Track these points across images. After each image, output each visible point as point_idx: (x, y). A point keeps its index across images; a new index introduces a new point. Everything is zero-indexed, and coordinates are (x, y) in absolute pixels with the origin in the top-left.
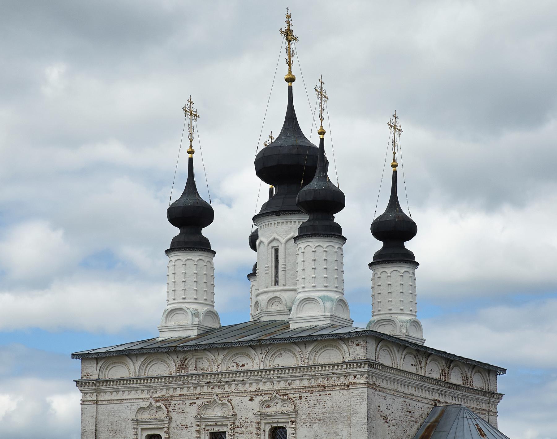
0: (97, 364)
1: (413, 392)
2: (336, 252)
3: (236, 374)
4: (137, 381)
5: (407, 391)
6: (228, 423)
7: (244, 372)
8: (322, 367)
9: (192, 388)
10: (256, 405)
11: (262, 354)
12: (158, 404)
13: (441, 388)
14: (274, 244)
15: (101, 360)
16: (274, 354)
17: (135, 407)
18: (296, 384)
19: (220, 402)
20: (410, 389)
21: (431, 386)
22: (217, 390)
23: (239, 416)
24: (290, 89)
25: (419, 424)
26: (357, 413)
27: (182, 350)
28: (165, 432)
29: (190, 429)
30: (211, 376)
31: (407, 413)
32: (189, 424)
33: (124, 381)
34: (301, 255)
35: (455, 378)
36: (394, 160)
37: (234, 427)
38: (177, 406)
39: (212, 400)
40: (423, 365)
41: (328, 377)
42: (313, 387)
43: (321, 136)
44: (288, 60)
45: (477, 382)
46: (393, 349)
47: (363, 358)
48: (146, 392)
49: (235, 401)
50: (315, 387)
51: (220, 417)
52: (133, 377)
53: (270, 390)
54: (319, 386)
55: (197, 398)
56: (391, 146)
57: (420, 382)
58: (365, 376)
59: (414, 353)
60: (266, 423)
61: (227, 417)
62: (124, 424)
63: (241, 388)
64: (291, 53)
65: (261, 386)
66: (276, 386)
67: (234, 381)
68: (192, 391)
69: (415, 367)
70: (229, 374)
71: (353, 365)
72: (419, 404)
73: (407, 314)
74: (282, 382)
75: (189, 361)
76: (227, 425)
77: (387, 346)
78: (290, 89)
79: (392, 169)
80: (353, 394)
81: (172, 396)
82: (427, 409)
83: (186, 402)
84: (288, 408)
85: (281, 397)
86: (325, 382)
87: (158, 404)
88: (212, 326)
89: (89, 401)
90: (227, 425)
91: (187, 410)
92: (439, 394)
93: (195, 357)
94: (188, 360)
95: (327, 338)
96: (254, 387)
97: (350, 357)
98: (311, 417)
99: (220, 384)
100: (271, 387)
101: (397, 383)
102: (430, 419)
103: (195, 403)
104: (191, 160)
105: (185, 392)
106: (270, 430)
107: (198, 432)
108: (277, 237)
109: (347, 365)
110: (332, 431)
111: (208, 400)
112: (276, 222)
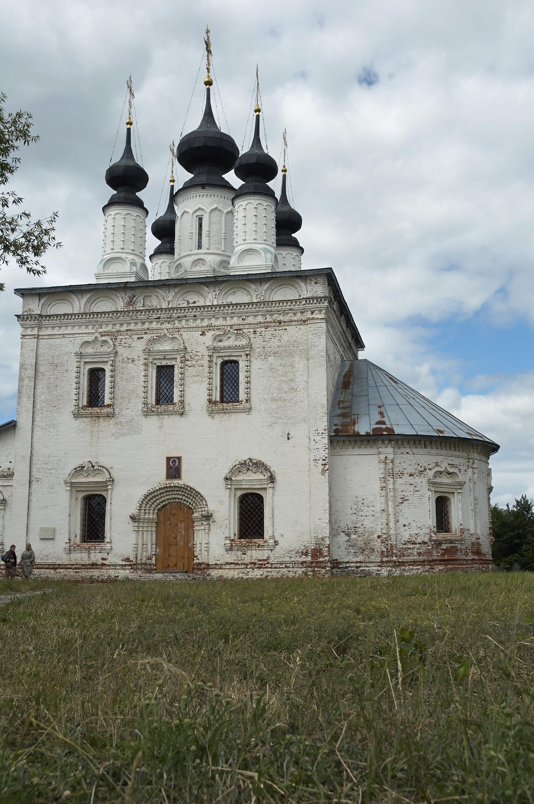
10: (208, 339)
11: (215, 291)
12: (104, 338)
14: (199, 213)
17: (79, 341)
18: (250, 320)
22: (166, 325)
23: (189, 350)
24: (208, 90)
29: (136, 363)
32: (136, 358)
36: (284, 166)
37: (184, 360)
41: (284, 313)
42: (268, 322)
50: (270, 322)
52: (75, 312)
54: (274, 322)
55: (146, 333)
61: (177, 351)
63: (191, 324)
65: (213, 322)
66: (229, 322)
71: (313, 301)
74: (236, 318)
75: (137, 299)
76: (176, 358)
78: (208, 90)
80: (311, 329)
81: (118, 331)
83: (133, 336)
84: (244, 342)
86: (281, 318)
87: (104, 338)
89: (29, 335)
91: (134, 344)
96: (205, 323)
98: (265, 351)
99: (170, 320)
100: (224, 323)
103: (143, 338)
105: (132, 327)
107: (145, 364)
111: (157, 335)
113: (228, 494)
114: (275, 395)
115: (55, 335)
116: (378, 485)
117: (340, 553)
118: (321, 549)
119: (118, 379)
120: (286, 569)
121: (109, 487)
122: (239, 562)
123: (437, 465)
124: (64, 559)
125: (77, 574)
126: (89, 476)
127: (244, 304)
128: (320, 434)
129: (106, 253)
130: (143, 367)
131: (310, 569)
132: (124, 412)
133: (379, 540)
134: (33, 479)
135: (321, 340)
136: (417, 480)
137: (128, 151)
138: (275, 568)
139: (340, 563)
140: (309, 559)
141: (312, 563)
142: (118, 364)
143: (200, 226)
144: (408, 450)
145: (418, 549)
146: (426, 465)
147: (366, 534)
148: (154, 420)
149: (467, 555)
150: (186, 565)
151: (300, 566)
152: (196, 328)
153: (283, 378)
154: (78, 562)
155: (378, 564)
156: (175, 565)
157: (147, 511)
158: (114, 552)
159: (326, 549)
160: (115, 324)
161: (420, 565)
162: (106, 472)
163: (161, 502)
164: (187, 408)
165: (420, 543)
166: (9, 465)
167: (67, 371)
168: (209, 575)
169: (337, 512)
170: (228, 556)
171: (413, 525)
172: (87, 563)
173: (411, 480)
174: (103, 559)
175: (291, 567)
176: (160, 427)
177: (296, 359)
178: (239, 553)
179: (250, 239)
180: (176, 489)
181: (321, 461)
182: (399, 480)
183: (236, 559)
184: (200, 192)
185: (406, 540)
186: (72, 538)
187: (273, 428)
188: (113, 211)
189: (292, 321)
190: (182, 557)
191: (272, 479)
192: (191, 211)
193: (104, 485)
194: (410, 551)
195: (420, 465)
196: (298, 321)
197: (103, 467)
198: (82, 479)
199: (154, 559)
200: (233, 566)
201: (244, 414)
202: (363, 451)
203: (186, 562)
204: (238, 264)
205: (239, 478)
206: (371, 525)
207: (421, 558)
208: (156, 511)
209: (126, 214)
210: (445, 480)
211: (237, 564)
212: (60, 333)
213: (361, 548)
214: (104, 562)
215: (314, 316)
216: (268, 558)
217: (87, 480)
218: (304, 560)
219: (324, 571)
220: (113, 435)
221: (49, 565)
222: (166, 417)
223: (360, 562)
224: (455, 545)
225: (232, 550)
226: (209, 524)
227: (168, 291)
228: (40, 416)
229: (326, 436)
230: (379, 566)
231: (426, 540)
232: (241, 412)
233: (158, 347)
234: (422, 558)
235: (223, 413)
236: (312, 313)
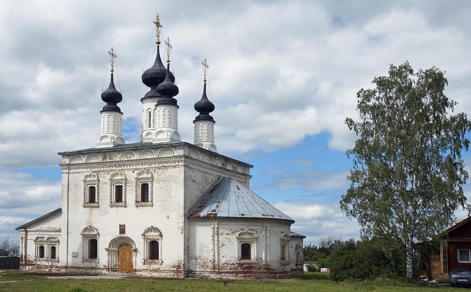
0: (69, 157)
1: (208, 171)
2: (174, 112)
3: (127, 161)
4: (85, 164)
5: (205, 170)
6: (123, 182)
7: (130, 160)
8: (164, 158)
9: (108, 167)
10: (135, 174)
11: (138, 153)
12: (94, 174)
13: (222, 170)
14: (149, 110)
15: (70, 156)
16: (143, 153)
17: (84, 175)
18: (153, 166)
19: (120, 173)
20: (206, 170)
21: (217, 169)
22: (119, 168)
23: (128, 179)
24: (158, 47)
25: (210, 185)
26: (179, 178)
27: (103, 151)
28: (97, 185)
29: (107, 184)
30: (116, 162)
31: (205, 180)
32: (107, 182)
33: (79, 165)
34: (158, 112)
35: (229, 167)
36: (205, 79)
37: (126, 183)
38: (102, 175)
39: (117, 172)
40: (213, 160)
41: (167, 162)
42: (160, 167)
43: (168, 63)
44: (157, 35)
45: (240, 170)
46: (198, 152)
47: (182, 154)
48: (89, 169)
49: (126, 173)
50: (161, 167)
51: (120, 179)
52: (83, 163)
53: (141, 168)
54: (163, 166)
55: (110, 172)
56: (203, 73)
57: (211, 167)
58: (183, 162)
59: (209, 155)
60: (140, 182)
61: (123, 180)
62: (79, 182)
63: (129, 167)
64: (159, 32)
65: (138, 167)
66: (144, 166)
67: (126, 164)
68: (108, 169)
69: (209, 161)
70: (124, 162)
71: (178, 157)
72: (211, 176)
73: (210, 142)
74: (147, 165)
75: (107, 156)
76: (123, 183)
77: (195, 151)
78: (158, 47)
79: (204, 82)
80: (178, 170)
81: (100, 171)
82: (215, 179)
83: (106, 173)
84: (150, 176)
85: (146, 171)
86: (166, 165)
87: (94, 174)
88: (121, 144)
89: (65, 172)
90: (123, 183)
91: (106, 176)
92: (221, 173)
93: (110, 154)
94: (107, 155)
95: (166, 146)
96: (135, 167)
97: (176, 154)
98: (159, 180)
99: (120, 166)
100: (142, 167)
101: (202, 167)
102: (216, 183)
103: (109, 174)
104: (112, 74)
105: (105, 169)
106: (141, 185)
107: (111, 185)
108: (150, 107)
109: (175, 157)
110: (168, 185)
111: (115, 172)
112: (150, 101)
113: (143, 241)
114: (163, 199)
115: (75, 172)
116: (211, 238)
117: (193, 267)
118: (180, 265)
119: (100, 191)
120: (167, 273)
121: (98, 236)
122: (148, 269)
123: (242, 229)
124: (81, 265)
125: (86, 271)
126: (90, 232)
127: (150, 159)
128: (181, 216)
129: (104, 133)
130: (109, 186)
131: (176, 273)
132: (103, 205)
133: (210, 262)
134: (69, 232)
135: (181, 175)
136: (231, 236)
137: (112, 84)
138: (162, 272)
139: (193, 271)
140: (176, 269)
141: (176, 271)
142: (100, 185)
143: (150, 116)
144: (226, 223)
145: (230, 266)
146: (236, 230)
147: (205, 259)
148: (114, 209)
149: (259, 269)
150: (130, 269)
151: (172, 272)
152: (131, 169)
153: (166, 192)
154: (87, 266)
155: (210, 272)
156: (126, 269)
157: (113, 247)
158: (100, 262)
159: (182, 265)
160: (99, 168)
161: (230, 274)
162: (96, 230)
163: (120, 243)
164: (127, 204)
165: (230, 264)
166: (60, 227)
167: (80, 188)
168: (136, 274)
169: (192, 249)
170: (144, 266)
171: (228, 256)
172: (90, 267)
173: (227, 236)
174: (96, 266)
175: (168, 272)
176: (117, 212)
177: (172, 183)
178: (148, 265)
179: (161, 126)
180: (118, 239)
181: (181, 228)
182: (221, 236)
183: (147, 268)
184: (149, 100)
185: (224, 262)
186: (85, 257)
187: (162, 213)
188: (104, 114)
189: (170, 166)
190: (128, 266)
191: (161, 235)
192: (146, 109)
193: (95, 235)
194: (225, 267)
195: (232, 230)
196: (173, 166)
197: (94, 228)
198: (86, 233)
199: (117, 266)
200: (145, 271)
201: (150, 207)
202: (204, 223)
203: (130, 268)
204: (156, 137)
205: (148, 234)
206: (207, 256)
207: (231, 270)
208: (118, 247)
209: (109, 115)
210: (247, 236)
211: (147, 270)
212: (77, 171)
213: (202, 265)
214: (96, 267)
215: (179, 164)
216: (160, 268)
217: (89, 233)
218: (174, 269)
219: (181, 274)
220: (99, 215)
221: (76, 267)
222: (119, 208)
223: (201, 271)
224: (251, 265)
225: (145, 264)
226: (136, 253)
227: (119, 153)
228: (71, 206)
229: (183, 217)
230: (210, 273)
231: (235, 263)
232: (149, 206)
233: (116, 178)
234: (231, 271)
235: (141, 206)
236: (178, 162)
